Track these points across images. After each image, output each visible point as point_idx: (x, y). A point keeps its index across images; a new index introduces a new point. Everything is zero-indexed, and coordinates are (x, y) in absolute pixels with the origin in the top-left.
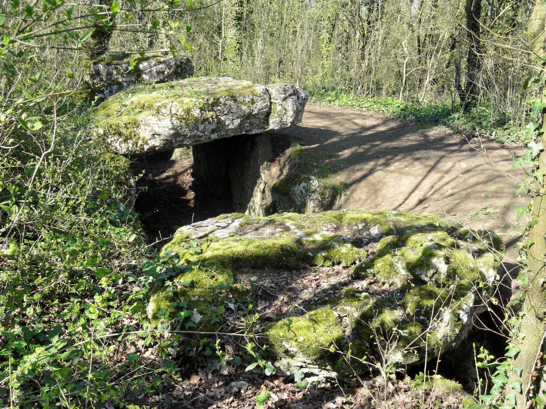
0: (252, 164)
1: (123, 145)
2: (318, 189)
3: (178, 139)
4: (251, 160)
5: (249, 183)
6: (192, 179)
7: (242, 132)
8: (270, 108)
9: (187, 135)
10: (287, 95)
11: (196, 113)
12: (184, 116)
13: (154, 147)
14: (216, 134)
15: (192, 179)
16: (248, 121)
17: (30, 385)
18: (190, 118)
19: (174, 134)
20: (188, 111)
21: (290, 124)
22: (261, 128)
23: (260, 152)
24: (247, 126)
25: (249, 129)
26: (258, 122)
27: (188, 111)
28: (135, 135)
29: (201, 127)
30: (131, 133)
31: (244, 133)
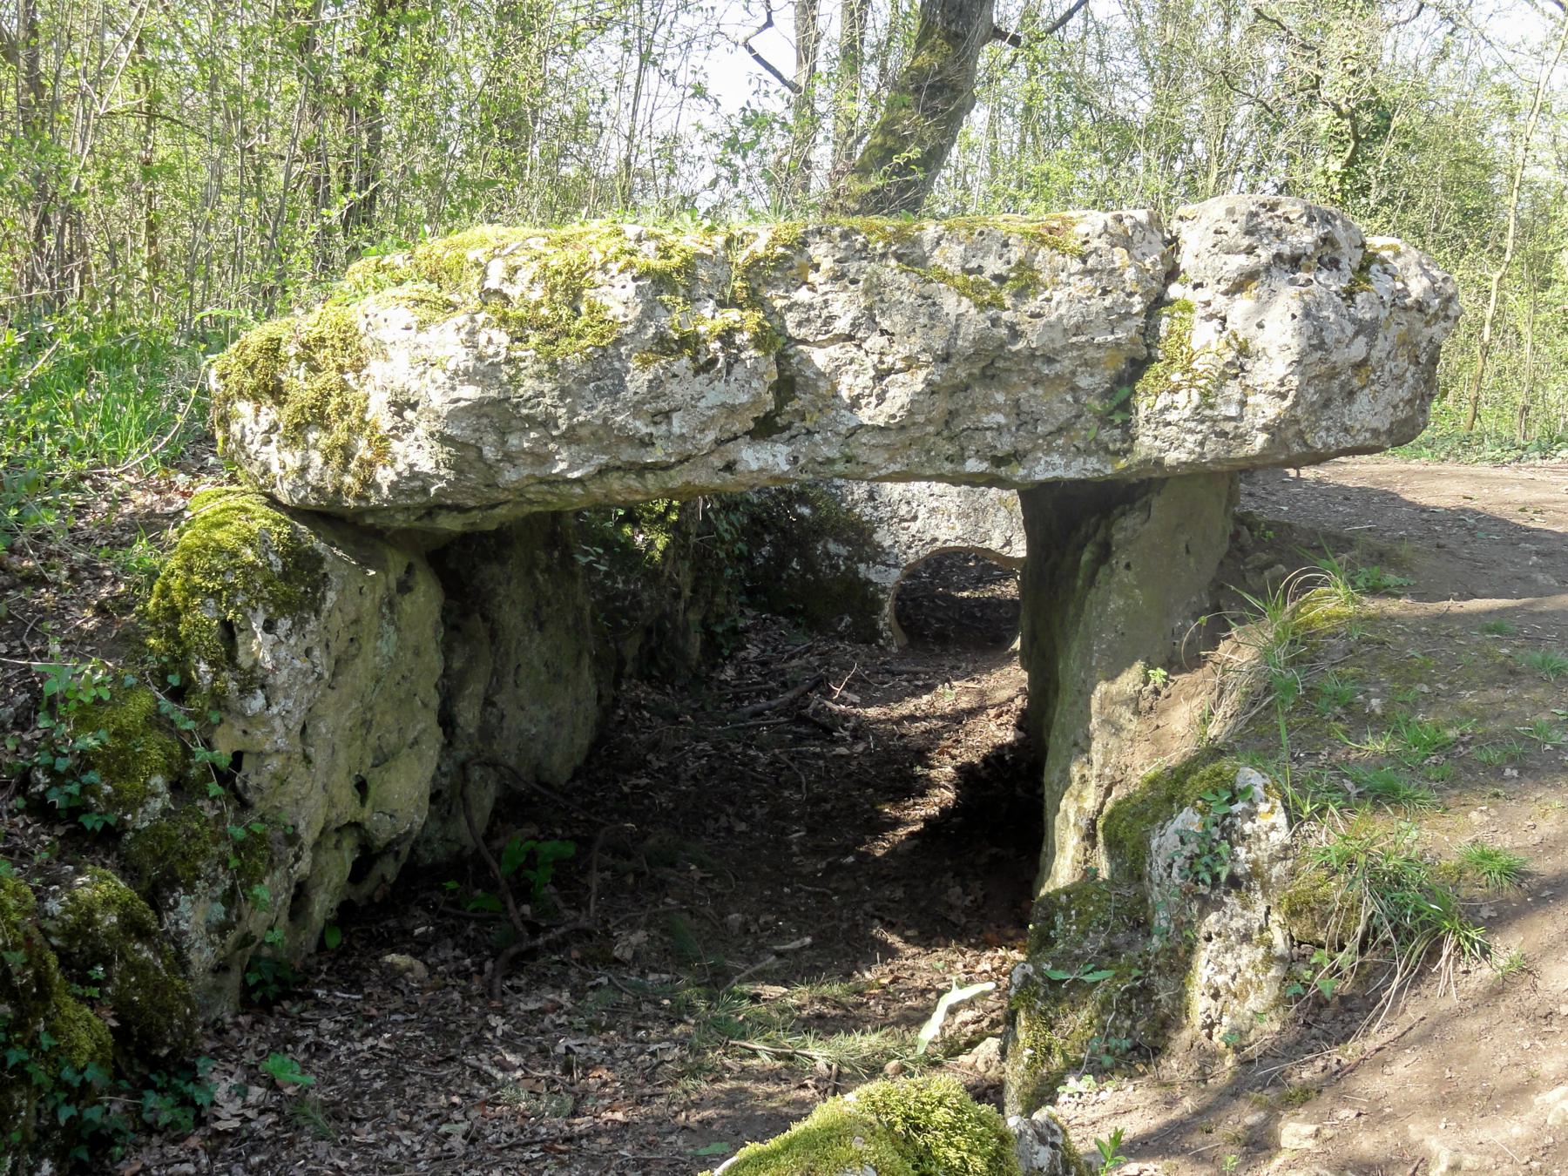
2: (1278, 870)
3: (513, 440)
8: (1149, 331)
10: (1265, 255)
11: (617, 299)
14: (783, 451)
19: (478, 409)
20: (572, 287)
21: (1260, 440)
22: (1087, 452)
23: (1117, 602)
24: (999, 429)
25: (1005, 445)
26: (1064, 412)
27: (572, 287)
28: (344, 410)
29: (638, 380)
30: (325, 395)
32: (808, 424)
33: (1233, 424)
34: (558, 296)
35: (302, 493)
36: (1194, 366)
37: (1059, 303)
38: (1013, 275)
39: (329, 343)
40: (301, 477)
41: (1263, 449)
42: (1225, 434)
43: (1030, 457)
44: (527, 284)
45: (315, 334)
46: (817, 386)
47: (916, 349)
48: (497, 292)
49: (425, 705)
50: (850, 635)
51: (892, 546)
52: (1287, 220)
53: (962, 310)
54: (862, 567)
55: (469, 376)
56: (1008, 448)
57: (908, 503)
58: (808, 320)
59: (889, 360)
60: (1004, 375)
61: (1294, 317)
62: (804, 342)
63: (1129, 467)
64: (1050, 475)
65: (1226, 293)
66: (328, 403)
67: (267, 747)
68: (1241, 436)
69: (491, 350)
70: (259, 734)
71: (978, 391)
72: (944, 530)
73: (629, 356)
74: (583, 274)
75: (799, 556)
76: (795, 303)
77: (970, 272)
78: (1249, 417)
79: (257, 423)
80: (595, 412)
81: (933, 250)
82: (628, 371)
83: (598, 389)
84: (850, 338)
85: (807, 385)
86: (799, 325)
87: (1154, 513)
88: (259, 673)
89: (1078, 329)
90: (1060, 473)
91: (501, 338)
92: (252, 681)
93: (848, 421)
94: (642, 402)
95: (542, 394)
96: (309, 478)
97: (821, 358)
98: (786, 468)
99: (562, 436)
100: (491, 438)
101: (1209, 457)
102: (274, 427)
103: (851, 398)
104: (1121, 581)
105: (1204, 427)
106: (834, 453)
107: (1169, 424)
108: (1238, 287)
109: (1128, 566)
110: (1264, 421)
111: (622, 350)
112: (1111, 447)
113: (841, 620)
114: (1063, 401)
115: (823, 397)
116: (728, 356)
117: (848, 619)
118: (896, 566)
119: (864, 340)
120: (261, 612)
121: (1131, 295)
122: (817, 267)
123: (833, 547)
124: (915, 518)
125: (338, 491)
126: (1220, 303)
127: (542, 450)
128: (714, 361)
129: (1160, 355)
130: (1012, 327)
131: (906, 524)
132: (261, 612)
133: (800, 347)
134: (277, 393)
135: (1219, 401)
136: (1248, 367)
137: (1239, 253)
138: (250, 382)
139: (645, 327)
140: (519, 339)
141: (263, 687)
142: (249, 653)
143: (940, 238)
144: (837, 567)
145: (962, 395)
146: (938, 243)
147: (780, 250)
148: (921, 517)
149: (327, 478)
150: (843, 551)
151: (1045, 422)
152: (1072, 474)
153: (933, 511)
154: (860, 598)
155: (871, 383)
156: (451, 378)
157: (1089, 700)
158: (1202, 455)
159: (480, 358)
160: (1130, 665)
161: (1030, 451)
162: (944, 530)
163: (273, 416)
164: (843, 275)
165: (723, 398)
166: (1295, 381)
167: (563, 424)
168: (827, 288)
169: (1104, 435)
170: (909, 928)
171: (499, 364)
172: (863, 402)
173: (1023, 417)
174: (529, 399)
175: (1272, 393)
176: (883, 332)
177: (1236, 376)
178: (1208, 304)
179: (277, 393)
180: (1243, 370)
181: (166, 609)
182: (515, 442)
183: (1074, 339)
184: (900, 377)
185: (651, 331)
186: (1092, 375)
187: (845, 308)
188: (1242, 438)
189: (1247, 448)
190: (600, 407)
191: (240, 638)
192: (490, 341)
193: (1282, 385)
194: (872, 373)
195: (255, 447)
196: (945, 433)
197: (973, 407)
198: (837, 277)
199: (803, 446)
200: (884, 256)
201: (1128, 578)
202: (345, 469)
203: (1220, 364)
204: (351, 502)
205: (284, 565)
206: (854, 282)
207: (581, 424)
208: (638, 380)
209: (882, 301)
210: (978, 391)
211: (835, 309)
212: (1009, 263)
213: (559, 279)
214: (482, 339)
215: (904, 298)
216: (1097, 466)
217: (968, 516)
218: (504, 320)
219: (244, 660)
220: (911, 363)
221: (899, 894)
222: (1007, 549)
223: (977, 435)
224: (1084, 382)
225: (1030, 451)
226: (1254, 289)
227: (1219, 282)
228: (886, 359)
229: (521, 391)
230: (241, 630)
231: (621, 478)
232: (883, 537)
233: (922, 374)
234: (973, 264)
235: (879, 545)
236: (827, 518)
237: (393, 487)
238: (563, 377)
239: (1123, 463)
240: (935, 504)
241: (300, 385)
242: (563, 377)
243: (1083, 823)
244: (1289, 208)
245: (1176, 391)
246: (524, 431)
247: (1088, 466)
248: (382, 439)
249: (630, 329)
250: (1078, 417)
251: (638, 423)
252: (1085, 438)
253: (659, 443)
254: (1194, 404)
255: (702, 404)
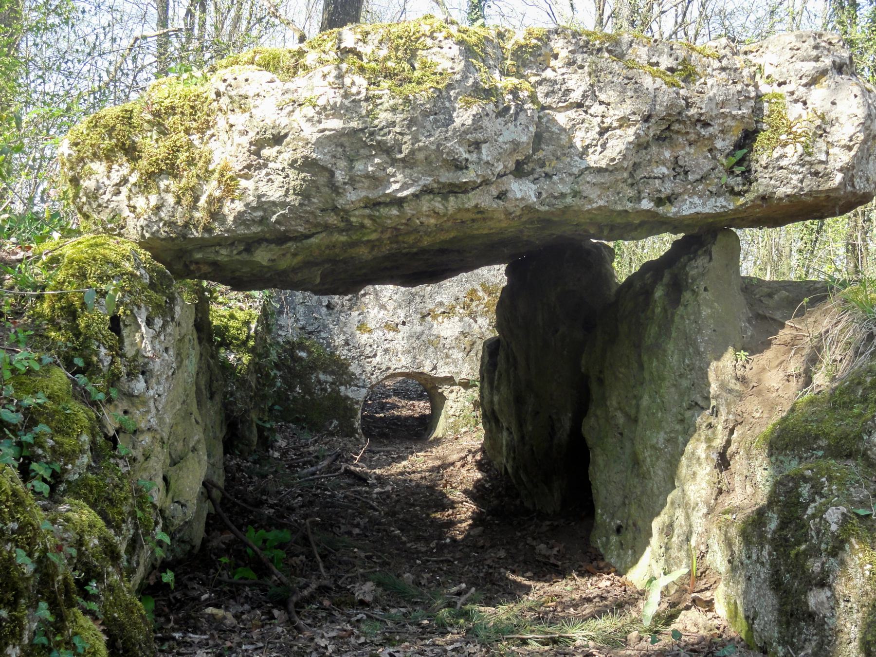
0: (673, 360)
1: (140, 202)
3: (359, 166)
4: (670, 347)
5: (660, 439)
6: (479, 475)
7: (639, 199)
9: (398, 146)
10: (827, 62)
12: (390, 64)
13: (264, 206)
15: (479, 475)
16: (667, 154)
17: (797, 555)
18: (417, 74)
19: (338, 139)
21: (839, 178)
22: (718, 195)
23: (705, 312)
24: (663, 178)
25: (667, 189)
26: (707, 165)
28: (191, 162)
29: (463, 117)
30: (175, 150)
31: (646, 204)
32: (547, 169)
33: (824, 166)
34: (400, 54)
35: (155, 228)
36: (794, 129)
37: (712, 86)
38: (680, 67)
39: (179, 110)
40: (156, 214)
41: (840, 184)
42: (816, 174)
43: (680, 199)
44: (376, 42)
45: (167, 103)
46: (559, 139)
47: (628, 112)
48: (352, 51)
49: (197, 422)
50: (338, 432)
51: (361, 374)
52: (830, 43)
53: (657, 85)
54: (342, 388)
55: (335, 111)
56: (669, 192)
57: (371, 346)
58: (553, 92)
59: (608, 121)
60: (674, 136)
61: (856, 96)
62: (550, 107)
63: (746, 203)
64: (693, 211)
65: (805, 85)
66: (177, 158)
67: (143, 425)
68: (828, 175)
69: (354, 90)
70: (137, 413)
71: (654, 149)
72: (394, 362)
73: (456, 98)
74: (418, 39)
75: (301, 383)
76: (545, 79)
77: (652, 65)
78: (831, 162)
79: (109, 178)
80: (432, 139)
81: (627, 50)
82: (454, 110)
83: (436, 121)
84: (579, 105)
85: (551, 139)
86: (547, 95)
87: (714, 256)
88: (141, 360)
89: (723, 104)
90: (699, 209)
91: (361, 82)
92: (140, 368)
93: (578, 165)
94: (466, 132)
95: (393, 124)
96: (163, 214)
97: (562, 119)
98: (535, 200)
99: (403, 160)
100: (342, 164)
101: (806, 190)
102: (125, 181)
103: (583, 147)
104: (705, 298)
105: (804, 169)
106: (566, 190)
107: (782, 168)
108: (814, 81)
109: (706, 289)
110: (841, 164)
111: (452, 93)
112: (736, 189)
113: (332, 423)
114: (706, 157)
115: (562, 147)
116: (517, 105)
117: (335, 422)
118: (364, 387)
119: (589, 107)
120: (143, 310)
121: (747, 85)
122: (556, 57)
123: (322, 377)
124: (375, 355)
125: (186, 225)
126: (801, 91)
127: (382, 174)
128: (508, 108)
129: (765, 127)
130: (686, 99)
131: (369, 360)
132: (143, 310)
133: (547, 111)
134: (132, 152)
135: (815, 150)
136: (828, 130)
137: (810, 60)
138: (107, 143)
139: (467, 77)
140: (374, 84)
141: (143, 373)
142: (133, 344)
143: (632, 42)
144: (325, 390)
145: (644, 152)
146: (631, 46)
147: (534, 41)
148: (379, 354)
149: (178, 215)
150: (330, 379)
151: (694, 172)
152: (707, 210)
153: (386, 351)
154: (341, 408)
155: (597, 136)
156: (319, 113)
157: (706, 373)
158: (802, 189)
159: (346, 96)
160: (726, 350)
161: (681, 194)
162: (394, 362)
163: (125, 171)
164: (574, 62)
165: (514, 136)
166: (861, 136)
167: (406, 149)
168: (564, 70)
169: (731, 181)
170: (526, 571)
171: (360, 101)
172: (591, 150)
173: (679, 169)
174: (381, 129)
175: (843, 147)
176: (601, 103)
177: (821, 136)
178: (792, 93)
179: (132, 152)
180: (825, 132)
181: (62, 308)
182: (361, 167)
183: (722, 110)
184: (618, 132)
185: (471, 81)
186: (724, 140)
187: (578, 84)
188: (828, 176)
189: (830, 183)
190: (437, 135)
191: (125, 332)
192: (353, 83)
193: (851, 140)
194: (598, 129)
195: (106, 197)
196: (630, 181)
197: (650, 161)
198: (570, 63)
199: (545, 185)
200: (599, 50)
201: (708, 296)
202: (194, 206)
203: (813, 127)
204: (196, 234)
205: (151, 277)
206: (581, 67)
207: (420, 149)
208: (463, 117)
209: (599, 81)
210: (654, 149)
211: (571, 84)
212: (677, 59)
213: (402, 42)
214: (347, 81)
215: (615, 79)
216: (724, 204)
217: (409, 352)
218: (362, 69)
219: (129, 351)
220: (624, 122)
221: (502, 554)
222: (434, 372)
223: (651, 181)
224: (719, 144)
225: (681, 194)
226: (825, 81)
227: (801, 78)
228: (605, 120)
229: (376, 122)
230: (126, 326)
231: (430, 201)
232: (354, 368)
233: (631, 131)
234: (654, 60)
235: (353, 374)
236: (318, 359)
237: (240, 218)
238: (413, 109)
239: (742, 200)
240: (388, 346)
241: (153, 146)
242: (413, 109)
243: (715, 456)
244: (830, 36)
245: (784, 146)
246: (370, 157)
247: (718, 204)
248: (232, 179)
249: (458, 77)
250: (713, 169)
251: (461, 149)
252: (717, 185)
253: (471, 166)
254: (799, 154)
255: (501, 139)
